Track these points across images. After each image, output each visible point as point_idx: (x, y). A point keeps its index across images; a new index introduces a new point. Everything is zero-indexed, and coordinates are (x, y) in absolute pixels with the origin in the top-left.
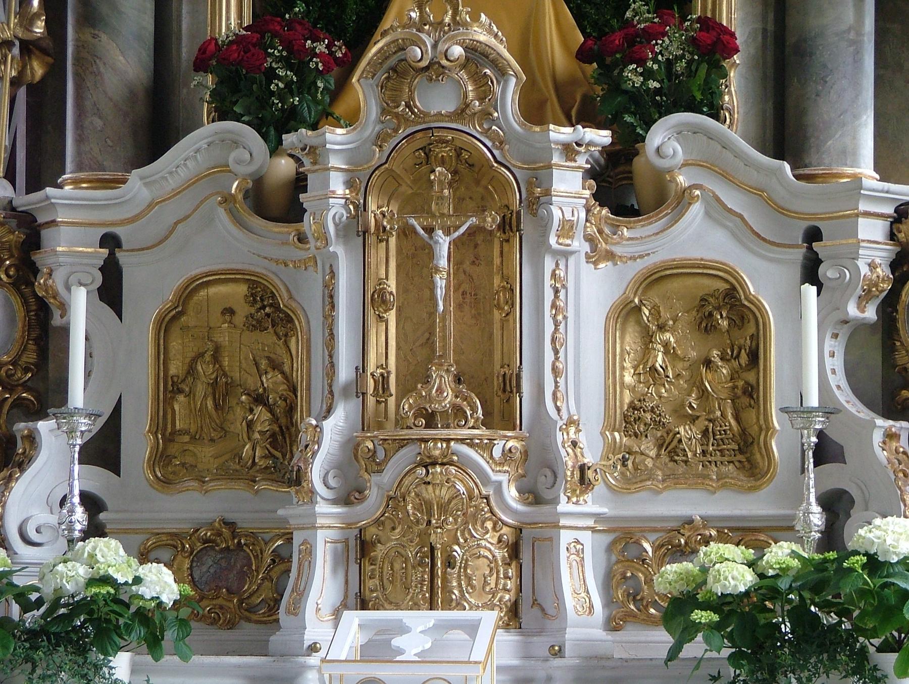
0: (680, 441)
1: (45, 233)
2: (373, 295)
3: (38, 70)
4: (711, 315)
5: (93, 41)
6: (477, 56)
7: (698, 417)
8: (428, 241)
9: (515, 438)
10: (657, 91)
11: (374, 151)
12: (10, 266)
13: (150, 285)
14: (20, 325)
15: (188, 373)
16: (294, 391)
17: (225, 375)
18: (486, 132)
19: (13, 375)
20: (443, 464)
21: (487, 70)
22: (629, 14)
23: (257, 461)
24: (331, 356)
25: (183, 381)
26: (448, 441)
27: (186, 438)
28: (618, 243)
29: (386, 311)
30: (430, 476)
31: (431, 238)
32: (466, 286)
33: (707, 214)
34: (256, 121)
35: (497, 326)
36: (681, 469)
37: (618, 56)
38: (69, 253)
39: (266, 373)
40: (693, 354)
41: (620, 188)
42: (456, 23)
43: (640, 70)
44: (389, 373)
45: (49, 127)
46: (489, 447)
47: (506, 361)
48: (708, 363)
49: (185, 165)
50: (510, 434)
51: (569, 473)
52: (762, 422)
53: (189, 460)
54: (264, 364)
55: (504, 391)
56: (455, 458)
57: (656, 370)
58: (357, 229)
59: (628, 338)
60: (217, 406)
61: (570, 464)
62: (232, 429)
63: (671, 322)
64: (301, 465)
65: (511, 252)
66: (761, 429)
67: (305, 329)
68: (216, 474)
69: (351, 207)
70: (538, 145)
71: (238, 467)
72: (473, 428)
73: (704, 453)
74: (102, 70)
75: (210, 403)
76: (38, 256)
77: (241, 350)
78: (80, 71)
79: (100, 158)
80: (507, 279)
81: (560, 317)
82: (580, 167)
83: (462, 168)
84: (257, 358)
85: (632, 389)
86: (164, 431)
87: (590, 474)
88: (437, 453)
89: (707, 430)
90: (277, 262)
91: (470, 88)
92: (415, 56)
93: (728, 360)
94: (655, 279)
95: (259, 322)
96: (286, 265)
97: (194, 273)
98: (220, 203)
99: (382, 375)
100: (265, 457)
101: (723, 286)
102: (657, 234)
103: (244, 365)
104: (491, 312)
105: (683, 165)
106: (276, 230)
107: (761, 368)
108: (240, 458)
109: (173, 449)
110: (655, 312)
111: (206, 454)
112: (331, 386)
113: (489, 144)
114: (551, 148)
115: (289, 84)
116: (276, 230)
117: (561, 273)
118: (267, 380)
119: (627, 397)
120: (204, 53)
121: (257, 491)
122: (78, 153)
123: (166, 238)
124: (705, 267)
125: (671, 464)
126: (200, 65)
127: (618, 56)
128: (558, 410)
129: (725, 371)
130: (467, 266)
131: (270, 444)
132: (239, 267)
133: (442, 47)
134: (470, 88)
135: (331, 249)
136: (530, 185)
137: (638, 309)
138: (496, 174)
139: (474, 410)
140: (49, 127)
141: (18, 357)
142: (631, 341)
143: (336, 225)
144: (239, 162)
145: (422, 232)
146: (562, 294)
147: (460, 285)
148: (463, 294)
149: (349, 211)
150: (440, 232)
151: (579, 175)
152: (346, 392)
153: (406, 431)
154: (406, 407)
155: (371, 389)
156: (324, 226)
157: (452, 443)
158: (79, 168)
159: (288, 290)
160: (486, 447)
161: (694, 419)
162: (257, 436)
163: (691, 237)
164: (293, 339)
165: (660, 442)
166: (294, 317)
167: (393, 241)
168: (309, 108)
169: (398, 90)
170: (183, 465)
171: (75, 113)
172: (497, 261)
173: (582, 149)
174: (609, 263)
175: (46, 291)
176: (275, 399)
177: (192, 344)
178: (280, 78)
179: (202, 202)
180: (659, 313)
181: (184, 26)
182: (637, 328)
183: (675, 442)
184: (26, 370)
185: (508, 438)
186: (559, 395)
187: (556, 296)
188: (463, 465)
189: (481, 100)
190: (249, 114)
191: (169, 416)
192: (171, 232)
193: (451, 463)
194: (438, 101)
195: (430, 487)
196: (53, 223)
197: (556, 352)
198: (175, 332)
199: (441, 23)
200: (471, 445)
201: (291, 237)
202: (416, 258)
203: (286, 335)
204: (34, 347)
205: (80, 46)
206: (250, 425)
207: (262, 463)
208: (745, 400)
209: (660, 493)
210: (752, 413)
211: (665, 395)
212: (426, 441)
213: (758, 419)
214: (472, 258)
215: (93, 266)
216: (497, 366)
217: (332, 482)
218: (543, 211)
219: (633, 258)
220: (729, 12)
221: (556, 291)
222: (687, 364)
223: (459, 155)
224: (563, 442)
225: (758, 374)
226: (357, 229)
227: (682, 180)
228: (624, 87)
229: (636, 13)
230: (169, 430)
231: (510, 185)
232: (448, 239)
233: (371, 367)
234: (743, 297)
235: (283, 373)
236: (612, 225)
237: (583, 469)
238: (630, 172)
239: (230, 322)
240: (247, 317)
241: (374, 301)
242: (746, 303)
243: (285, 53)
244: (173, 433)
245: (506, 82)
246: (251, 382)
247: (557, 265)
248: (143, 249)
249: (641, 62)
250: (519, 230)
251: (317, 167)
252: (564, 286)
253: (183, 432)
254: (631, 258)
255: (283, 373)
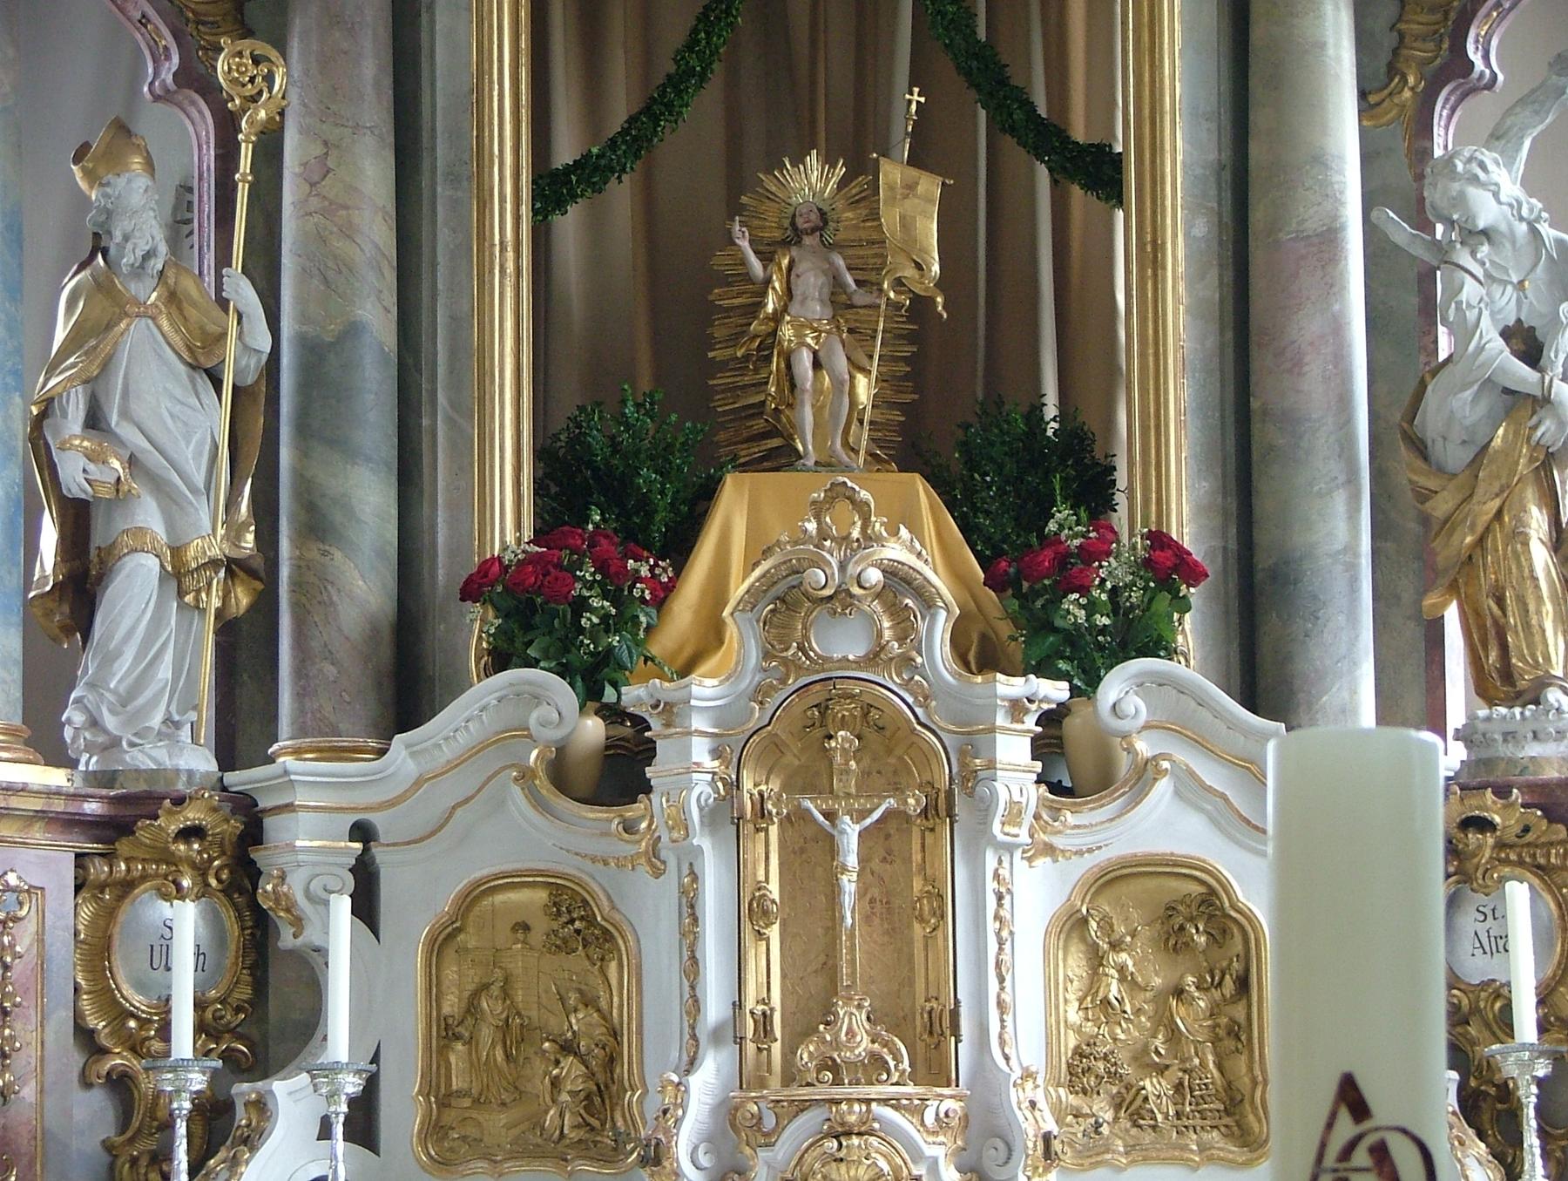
0: (1146, 1099)
1: (269, 822)
2: (750, 904)
3: (242, 599)
4: (1182, 928)
5: (323, 560)
6: (897, 578)
7: (1167, 1067)
8: (830, 830)
9: (952, 1097)
10: (1103, 630)
11: (752, 710)
12: (220, 868)
13: (419, 891)
14: (233, 947)
15: (468, 1011)
16: (615, 1034)
17: (519, 1014)
18: (906, 685)
19: (222, 1018)
20: (860, 1134)
21: (908, 601)
22: (1052, 526)
23: (566, 1131)
24: (693, 987)
25: (461, 1023)
26: (868, 1102)
27: (467, 1102)
28: (1060, 832)
29: (767, 926)
30: (844, 1151)
31: (833, 825)
32: (875, 892)
33: (1177, 793)
34: (560, 669)
35: (918, 946)
36: (1148, 1137)
37: (1046, 582)
38: (306, 847)
39: (576, 1011)
40: (1157, 981)
41: (1074, 767)
42: (869, 539)
43: (1083, 601)
44: (772, 1010)
45: (245, 677)
46: (919, 1112)
47: (932, 993)
48: (1179, 993)
49: (466, 728)
50: (946, 1091)
51: (1030, 1145)
52: (1257, 1072)
53: (471, 1131)
54: (573, 998)
55: (931, 1033)
56: (876, 1125)
57: (1109, 1003)
58: (733, 817)
59: (1070, 961)
60: (508, 1056)
61: (1031, 1133)
62: (529, 1089)
63: (1128, 939)
64: (660, 1136)
65: (938, 843)
66: (1255, 1083)
67: (634, 951)
68: (511, 1151)
69: (720, 784)
70: (979, 702)
71: (539, 1141)
72: (897, 1084)
73: (1178, 1115)
74: (335, 598)
75: (499, 1054)
76: (262, 853)
77: (538, 978)
78: (304, 600)
79: (333, 718)
80: (930, 880)
81: (1005, 934)
82: (1029, 731)
83: (866, 731)
84: (563, 992)
85: (1078, 1030)
86: (439, 1093)
87: (1056, 1146)
88: (852, 1119)
89: (1181, 1084)
90: (594, 860)
91: (886, 624)
92: (818, 582)
93: (1207, 990)
94: (1110, 879)
95: (565, 940)
96: (606, 863)
97: (478, 875)
98: (516, 779)
99: (764, 1013)
100: (578, 1127)
101: (1198, 889)
102: (1112, 820)
103: (544, 1001)
104: (910, 926)
105: (1147, 727)
106: (591, 815)
107: (1255, 998)
108: (543, 1128)
109: (450, 1117)
110: (1106, 925)
111: (497, 1124)
112: (693, 1028)
113: (910, 700)
114: (996, 705)
115: (605, 618)
116: (591, 815)
117: (1004, 872)
118: (578, 1021)
119: (1072, 1041)
120: (486, 575)
121: (570, 1174)
122: (300, 711)
123: (442, 827)
124: (1176, 865)
125: (1134, 1131)
126: (471, 590)
127: (1046, 582)
128: (1007, 1058)
129: (1202, 1004)
130: (876, 864)
131: (585, 1108)
132: (541, 866)
133: (853, 570)
134: (886, 624)
135: (695, 842)
136: (962, 753)
137: (1084, 921)
138: (915, 739)
139: (898, 1059)
140: (245, 677)
141: (230, 992)
142: (1075, 965)
143: (701, 809)
144: (543, 724)
145: (821, 818)
146: (1006, 901)
147: (866, 891)
148: (871, 902)
149: (717, 791)
150: (847, 818)
151: (1026, 743)
152: (717, 1036)
153: (810, 1089)
154: (805, 1056)
155: (750, 1034)
156: (683, 810)
157: (874, 1105)
158: (301, 731)
159: (609, 898)
160: (916, 1110)
161: (1162, 1070)
162: (565, 1097)
163: (1159, 825)
164: (613, 965)
165: (1118, 1100)
166: (616, 934)
167: (774, 830)
168: (630, 652)
169: (787, 626)
170: (464, 1138)
171: (294, 657)
172: (917, 857)
173: (1034, 707)
174: (1048, 859)
175: (277, 901)
176: (588, 1046)
177: (472, 972)
178: (592, 610)
179: (489, 779)
180: (1111, 926)
181: (441, 539)
182: (1082, 947)
183: (1139, 1101)
184: (238, 1010)
185: (941, 1097)
186: (1006, 1037)
187: (1000, 905)
188: (888, 1134)
189: (901, 639)
190: (547, 658)
191: (443, 1071)
192: (447, 820)
193: (871, 1133)
194: (842, 643)
195: (843, 1167)
196: (289, 808)
197: (1002, 980)
198: (450, 953)
199: (847, 538)
200: (896, 1108)
201: (614, 826)
202: (810, 852)
203: (602, 959)
204: (249, 979)
205: (300, 567)
206: (556, 1083)
207: (573, 1135)
208: (1230, 1044)
209: (1195, 1169)
210: (1242, 1060)
211: (1122, 1036)
212: (838, 1102)
213: (1251, 1069)
214: (882, 853)
215: (341, 866)
216: (920, 1000)
217: (704, 1161)
218: (982, 790)
219: (1080, 853)
220: (1180, 525)
221: (1000, 897)
222: (1149, 995)
223: (866, 715)
224: (1019, 1103)
225: (1249, 1006)
226: (733, 817)
227: (1144, 747)
228: (1059, 623)
229: (1061, 527)
230: (443, 1090)
231: (936, 754)
232: (857, 828)
233: (750, 1004)
234: (1227, 904)
235: (599, 1010)
236: (1051, 808)
237: (1047, 1138)
238: (1060, 738)
239: (524, 942)
240: (548, 935)
241: (751, 912)
242: (1233, 914)
243: (598, 577)
244: (449, 1095)
245: (933, 618)
246: (554, 1023)
247: (1000, 862)
248: (408, 843)
249: (1084, 590)
250: (951, 815)
251: (673, 730)
252: (1009, 891)
253: (461, 1094)
254: (1076, 853)
255: (599, 1010)
